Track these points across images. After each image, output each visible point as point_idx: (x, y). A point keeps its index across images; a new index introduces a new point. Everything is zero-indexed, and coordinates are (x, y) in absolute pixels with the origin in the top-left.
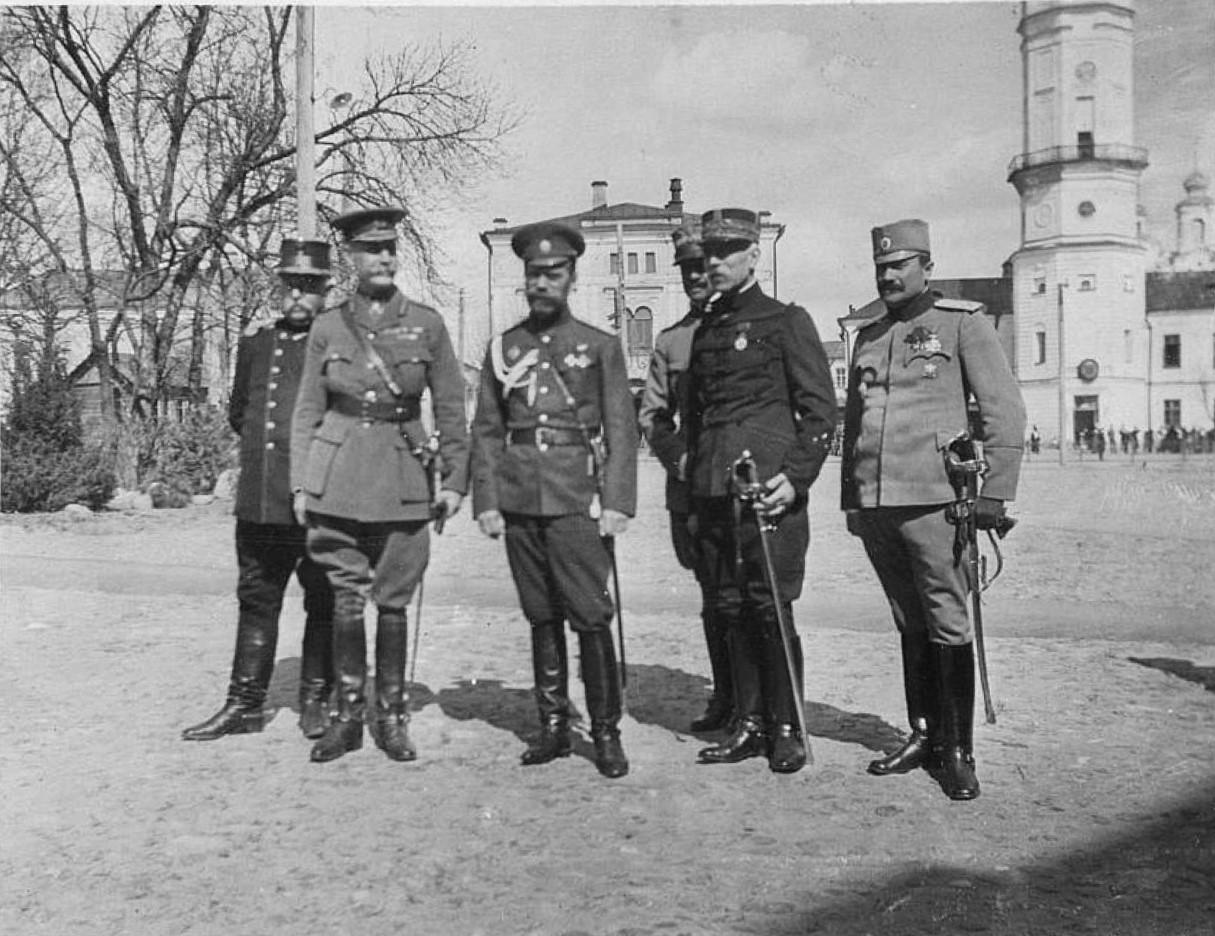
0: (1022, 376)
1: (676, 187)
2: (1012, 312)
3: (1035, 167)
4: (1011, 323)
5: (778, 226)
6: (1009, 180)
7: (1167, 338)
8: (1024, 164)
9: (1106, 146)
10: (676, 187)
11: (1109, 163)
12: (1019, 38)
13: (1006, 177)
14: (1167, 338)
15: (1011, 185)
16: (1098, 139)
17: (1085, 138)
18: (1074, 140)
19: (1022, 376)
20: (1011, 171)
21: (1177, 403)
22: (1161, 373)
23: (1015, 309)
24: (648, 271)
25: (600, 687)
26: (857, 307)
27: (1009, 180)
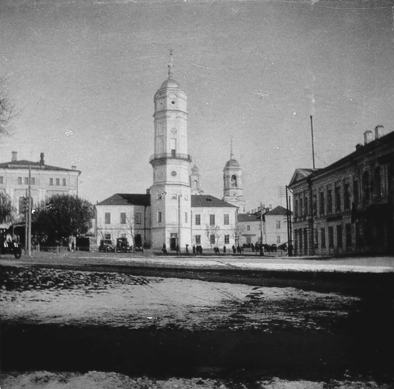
0: (154, 226)
1: (42, 155)
2: (150, 205)
3: (158, 159)
4: (150, 209)
5: (79, 171)
6: (150, 163)
7: (196, 216)
8: (154, 158)
9: (180, 154)
10: (42, 155)
11: (180, 158)
12: (153, 119)
13: (149, 161)
14: (196, 216)
15: (150, 164)
16: (177, 152)
17: (174, 152)
18: (170, 152)
19: (154, 226)
20: (151, 160)
21: (199, 236)
22: (195, 227)
23: (151, 204)
24: (63, 185)
25: (310, 251)
26: (99, 202)
27: (150, 163)
